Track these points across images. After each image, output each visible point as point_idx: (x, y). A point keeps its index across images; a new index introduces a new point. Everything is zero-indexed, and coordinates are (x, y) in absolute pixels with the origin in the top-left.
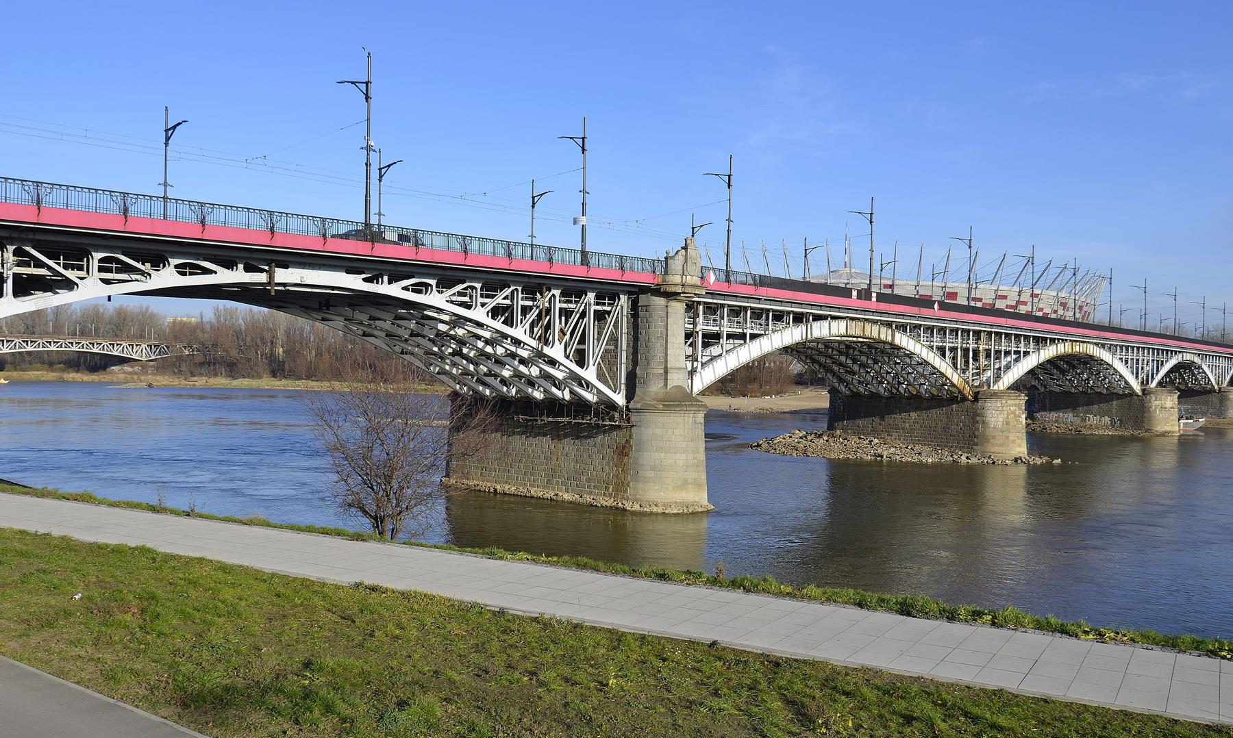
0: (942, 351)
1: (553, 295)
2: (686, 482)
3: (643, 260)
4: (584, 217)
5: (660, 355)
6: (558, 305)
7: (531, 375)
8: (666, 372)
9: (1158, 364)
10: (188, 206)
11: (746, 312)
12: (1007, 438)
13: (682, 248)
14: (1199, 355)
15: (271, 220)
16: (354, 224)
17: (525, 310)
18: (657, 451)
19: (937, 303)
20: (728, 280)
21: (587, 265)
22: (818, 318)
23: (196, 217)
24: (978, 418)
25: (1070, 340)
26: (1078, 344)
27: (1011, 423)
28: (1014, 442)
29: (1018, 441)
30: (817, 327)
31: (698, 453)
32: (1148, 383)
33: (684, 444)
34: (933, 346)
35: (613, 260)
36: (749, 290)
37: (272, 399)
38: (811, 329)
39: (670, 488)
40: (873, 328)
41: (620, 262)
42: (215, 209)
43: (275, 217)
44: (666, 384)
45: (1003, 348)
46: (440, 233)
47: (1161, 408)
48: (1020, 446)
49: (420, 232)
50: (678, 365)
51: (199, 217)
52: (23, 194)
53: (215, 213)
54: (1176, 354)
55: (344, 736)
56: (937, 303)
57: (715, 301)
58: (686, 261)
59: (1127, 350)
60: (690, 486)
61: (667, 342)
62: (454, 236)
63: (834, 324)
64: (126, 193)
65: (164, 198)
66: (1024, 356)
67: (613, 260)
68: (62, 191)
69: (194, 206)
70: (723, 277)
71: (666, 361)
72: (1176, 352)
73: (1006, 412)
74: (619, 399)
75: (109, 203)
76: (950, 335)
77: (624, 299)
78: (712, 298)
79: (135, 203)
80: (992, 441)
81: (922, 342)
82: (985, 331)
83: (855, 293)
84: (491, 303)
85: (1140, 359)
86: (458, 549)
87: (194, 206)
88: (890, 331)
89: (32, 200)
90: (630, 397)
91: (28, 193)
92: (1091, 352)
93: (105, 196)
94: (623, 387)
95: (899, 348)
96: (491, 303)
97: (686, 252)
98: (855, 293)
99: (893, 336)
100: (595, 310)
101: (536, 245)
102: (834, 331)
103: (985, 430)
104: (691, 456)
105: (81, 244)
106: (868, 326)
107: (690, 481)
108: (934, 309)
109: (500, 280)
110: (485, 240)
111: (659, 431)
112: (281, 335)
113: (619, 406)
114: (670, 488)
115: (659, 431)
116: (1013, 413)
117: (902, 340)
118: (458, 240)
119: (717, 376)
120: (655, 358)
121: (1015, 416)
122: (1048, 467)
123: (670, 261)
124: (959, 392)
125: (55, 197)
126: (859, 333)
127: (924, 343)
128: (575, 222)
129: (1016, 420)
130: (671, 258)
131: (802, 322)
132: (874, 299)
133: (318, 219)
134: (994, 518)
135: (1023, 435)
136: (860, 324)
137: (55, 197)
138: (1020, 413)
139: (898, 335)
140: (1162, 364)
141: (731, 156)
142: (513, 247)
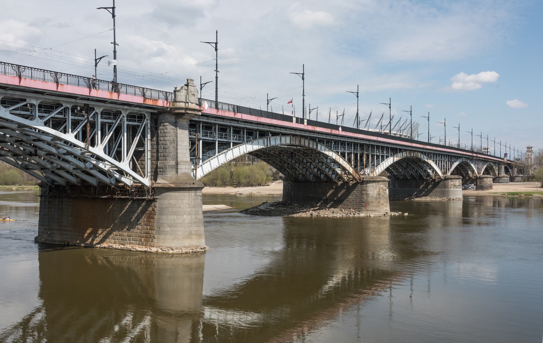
0: (343, 155)
1: (96, 113)
2: (191, 234)
3: (229, 105)
4: (115, 60)
5: (172, 154)
6: (100, 120)
7: (86, 168)
8: (177, 164)
12: (379, 202)
13: (185, 85)
14: (428, 155)
15: (56, 77)
16: (125, 85)
18: (172, 214)
19: (340, 127)
20: (217, 108)
21: (118, 92)
22: (274, 134)
24: (364, 192)
25: (409, 150)
26: (413, 152)
27: (381, 194)
28: (383, 204)
29: (385, 204)
30: (273, 140)
31: (198, 214)
32: (446, 173)
33: (189, 210)
35: (230, 107)
36: (231, 115)
38: (270, 140)
39: (181, 238)
40: (306, 141)
41: (233, 108)
42: (26, 69)
44: (177, 172)
45: (232, 141)
47: (454, 185)
48: (386, 206)
49: (145, 89)
50: (185, 160)
52: (13, 71)
53: (63, 78)
54: (436, 155)
58: (188, 93)
59: (442, 156)
60: (193, 236)
61: (177, 145)
63: (283, 138)
64: (57, 72)
66: (386, 158)
67: (230, 107)
70: (213, 105)
71: (177, 157)
72: (459, 157)
74: (147, 181)
75: (50, 77)
76: (348, 146)
80: (371, 204)
82: (366, 144)
83: (294, 119)
84: (48, 117)
87: (15, 67)
88: (315, 143)
89: (17, 74)
90: (155, 177)
91: (53, 77)
92: (419, 157)
93: (48, 73)
94: (149, 174)
96: (48, 117)
97: (188, 88)
98: (294, 119)
99: (317, 146)
100: (101, 122)
101: (99, 80)
102: (283, 142)
103: (367, 199)
104: (194, 217)
106: (302, 140)
107: (193, 232)
109: (54, 100)
111: (173, 202)
113: (146, 186)
114: (181, 238)
115: (173, 202)
116: (382, 188)
119: (213, 168)
120: (169, 155)
121: (383, 190)
122: (402, 217)
123: (177, 93)
124: (353, 178)
125: (63, 79)
126: (297, 143)
127: (334, 150)
128: (109, 63)
129: (384, 192)
130: (178, 91)
131: (265, 136)
132: (306, 124)
133: (15, 66)
135: (387, 200)
136: (298, 139)
137: (63, 79)
138: (385, 188)
139: (319, 146)
141: (217, 31)
142: (169, 95)
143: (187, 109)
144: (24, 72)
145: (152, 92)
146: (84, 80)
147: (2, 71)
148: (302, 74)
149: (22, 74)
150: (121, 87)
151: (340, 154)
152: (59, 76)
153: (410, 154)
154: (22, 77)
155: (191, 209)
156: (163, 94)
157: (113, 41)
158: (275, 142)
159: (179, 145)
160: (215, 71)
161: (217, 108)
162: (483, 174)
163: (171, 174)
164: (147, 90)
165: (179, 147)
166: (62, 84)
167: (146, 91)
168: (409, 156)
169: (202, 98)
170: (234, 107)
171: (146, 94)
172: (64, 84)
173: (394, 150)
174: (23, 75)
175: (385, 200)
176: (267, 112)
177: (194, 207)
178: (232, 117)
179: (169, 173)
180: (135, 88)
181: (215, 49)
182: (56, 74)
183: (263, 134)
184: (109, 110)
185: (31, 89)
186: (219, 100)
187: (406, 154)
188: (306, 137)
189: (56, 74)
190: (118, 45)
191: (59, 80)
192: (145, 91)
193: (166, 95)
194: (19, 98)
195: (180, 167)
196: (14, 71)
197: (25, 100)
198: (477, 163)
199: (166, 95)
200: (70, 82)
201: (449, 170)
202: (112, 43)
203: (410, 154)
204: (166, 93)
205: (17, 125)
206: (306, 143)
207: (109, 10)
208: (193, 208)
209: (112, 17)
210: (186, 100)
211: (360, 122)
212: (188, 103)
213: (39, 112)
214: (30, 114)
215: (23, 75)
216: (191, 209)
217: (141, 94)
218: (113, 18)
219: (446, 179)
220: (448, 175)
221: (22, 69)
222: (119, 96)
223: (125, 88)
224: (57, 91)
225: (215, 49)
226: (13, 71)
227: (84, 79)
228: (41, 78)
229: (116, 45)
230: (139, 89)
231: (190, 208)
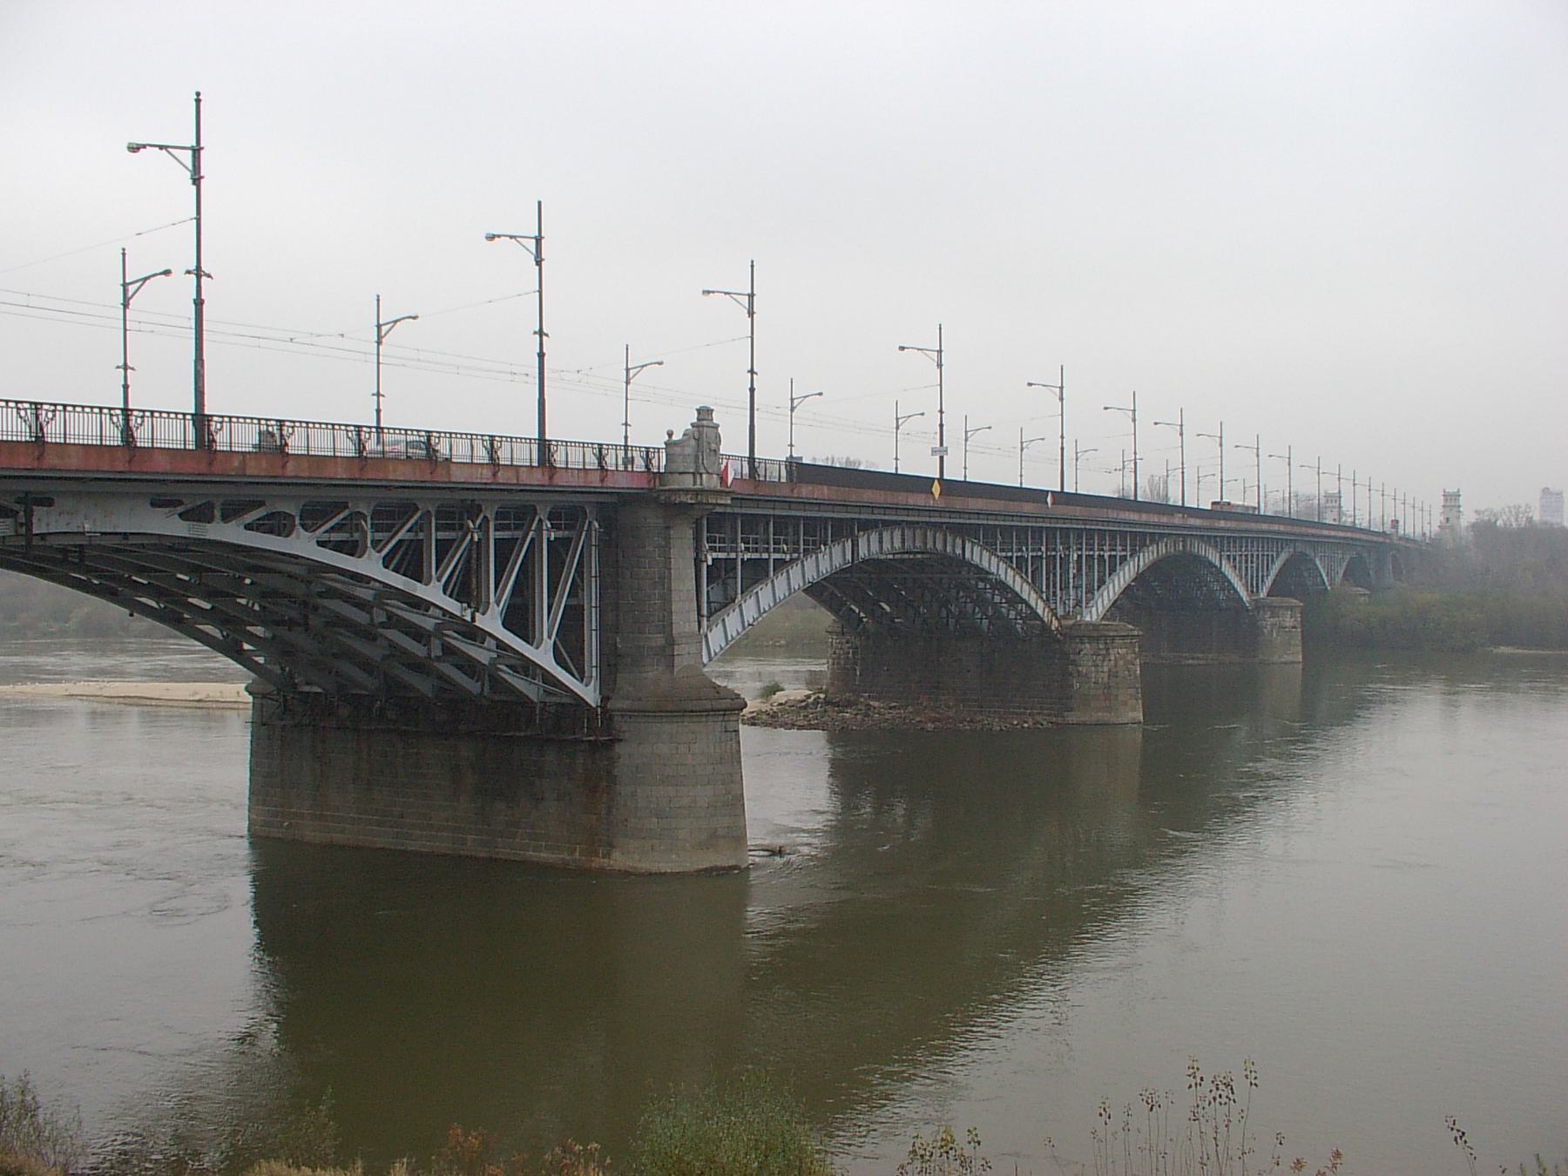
0: (1020, 566)
8: (671, 642)
9: (1268, 560)
10: (15, 410)
11: (768, 524)
15: (37, 418)
17: (444, 548)
22: (866, 526)
23: (28, 430)
28: (1125, 703)
34: (1012, 557)
37: (1454, 698)
41: (489, 446)
43: (44, 412)
46: (83, 407)
51: (34, 429)
52: (23, 426)
56: (1050, 494)
57: (793, 513)
62: (343, 427)
65: (624, 446)
67: (478, 444)
73: (1112, 658)
74: (589, 693)
78: (919, 516)
79: (52, 419)
81: (999, 554)
85: (1255, 554)
88: (959, 541)
95: (970, 565)
101: (632, 447)
107: (721, 832)
108: (1047, 503)
116: (1123, 657)
117: (977, 555)
118: (23, 413)
133: (27, 406)
140: (1272, 560)
141: (198, 94)
142: (139, 421)
143: (697, 492)
144: (54, 422)
147: (5, 429)
148: (192, 148)
150: (290, 430)
151: (1014, 566)
152: (47, 414)
153: (1175, 546)
155: (714, 769)
156: (115, 419)
157: (193, 267)
158: (869, 546)
159: (675, 590)
160: (535, 333)
162: (1268, 595)
163: (653, 673)
165: (675, 596)
167: (50, 415)
168: (1172, 550)
170: (492, 445)
173: (1139, 540)
175: (1132, 691)
176: (897, 474)
177: (721, 763)
179: (649, 669)
181: (189, 174)
182: (281, 426)
183: (843, 530)
186: (629, 444)
187: (881, 542)
188: (936, 526)
189: (281, 426)
190: (209, 276)
193: (359, 435)
195: (678, 650)
196: (23, 424)
197: (261, 504)
198: (1263, 547)
199: (359, 435)
200: (108, 435)
201: (1263, 581)
202: (189, 272)
203: (1175, 546)
204: (37, 406)
205: (374, 592)
206: (936, 542)
207: (176, 156)
208: (719, 766)
209: (191, 181)
210: (697, 467)
212: (701, 474)
215: (49, 432)
216: (714, 769)
218: (194, 183)
219: (1259, 606)
220: (1262, 596)
225: (749, 313)
226: (23, 426)
227: (18, 409)
228: (92, 436)
229: (204, 279)
231: (712, 766)
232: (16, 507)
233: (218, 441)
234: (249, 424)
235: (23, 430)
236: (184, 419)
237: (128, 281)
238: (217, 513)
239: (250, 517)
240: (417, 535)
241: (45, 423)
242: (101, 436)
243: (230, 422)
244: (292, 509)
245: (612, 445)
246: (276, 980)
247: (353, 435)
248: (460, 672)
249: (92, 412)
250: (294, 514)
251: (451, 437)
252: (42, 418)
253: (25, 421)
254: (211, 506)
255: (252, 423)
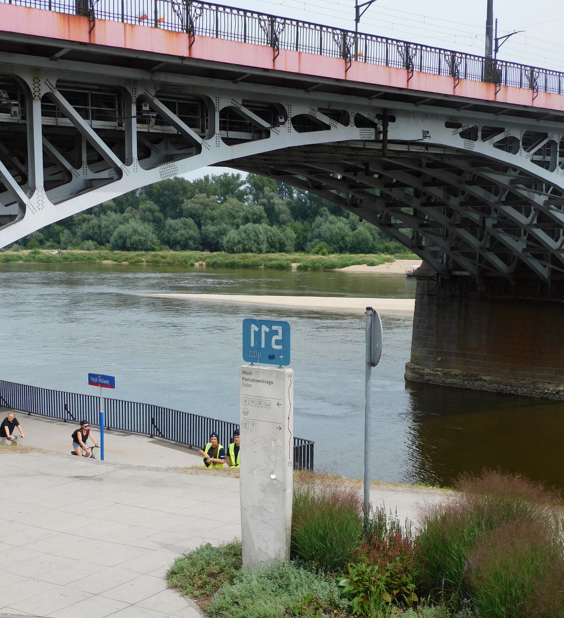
15: (188, 13)
20: (533, 86)
23: (180, 23)
35: (393, 49)
49: (278, 20)
55: (214, 616)
62: (330, 30)
68: (254, 20)
69: (338, 34)
77: (364, 167)
79: (200, 15)
86: (97, 308)
89: (182, 26)
100: (86, 94)
105: (194, 87)
110: (307, 25)
112: (262, 237)
134: (74, 277)
144: (201, 17)
145: (221, 16)
146: (334, 37)
149: (95, 8)
154: (96, 16)
156: (336, 37)
161: (533, 86)
164: (284, 24)
166: (103, 18)
169: (359, 31)
170: (532, 74)
171: (280, 37)
172: (107, 18)
174: (99, 9)
178: (525, 106)
180: (245, 16)
184: (255, 102)
185: (552, 113)
191: (197, 24)
192: (278, 27)
193: (272, 25)
194: (99, 82)
196: (177, 17)
197: (501, 130)
199: (272, 25)
204: (407, 44)
211: (500, 42)
213: (43, 114)
214: (20, 122)
217: (337, 48)
221: (278, 26)
222: (91, 30)
223: (241, 20)
224: (274, 71)
227: (260, 19)
230: (334, 34)
232: (376, 121)
233: (280, 40)
234: (551, 75)
235: (263, 38)
236: (440, 53)
237: (359, 4)
238: (479, 134)
239: (498, 138)
240: (544, 158)
241: (194, 18)
242: (123, 15)
243: (466, 58)
244: (518, 134)
245: (543, 69)
246: (461, 514)
247: (402, 50)
248: (198, 251)
249: (239, 15)
250: (519, 139)
251: (506, 65)
252: (192, 13)
253: (178, 15)
254: (475, 130)
255: (475, 60)
